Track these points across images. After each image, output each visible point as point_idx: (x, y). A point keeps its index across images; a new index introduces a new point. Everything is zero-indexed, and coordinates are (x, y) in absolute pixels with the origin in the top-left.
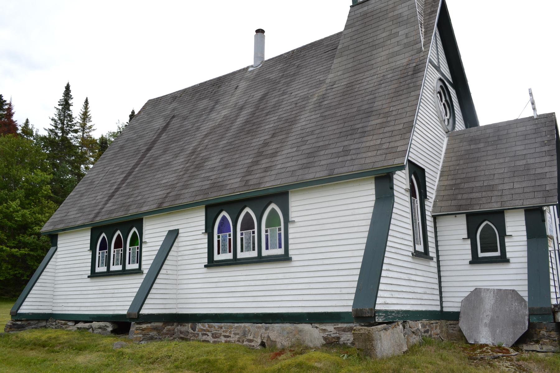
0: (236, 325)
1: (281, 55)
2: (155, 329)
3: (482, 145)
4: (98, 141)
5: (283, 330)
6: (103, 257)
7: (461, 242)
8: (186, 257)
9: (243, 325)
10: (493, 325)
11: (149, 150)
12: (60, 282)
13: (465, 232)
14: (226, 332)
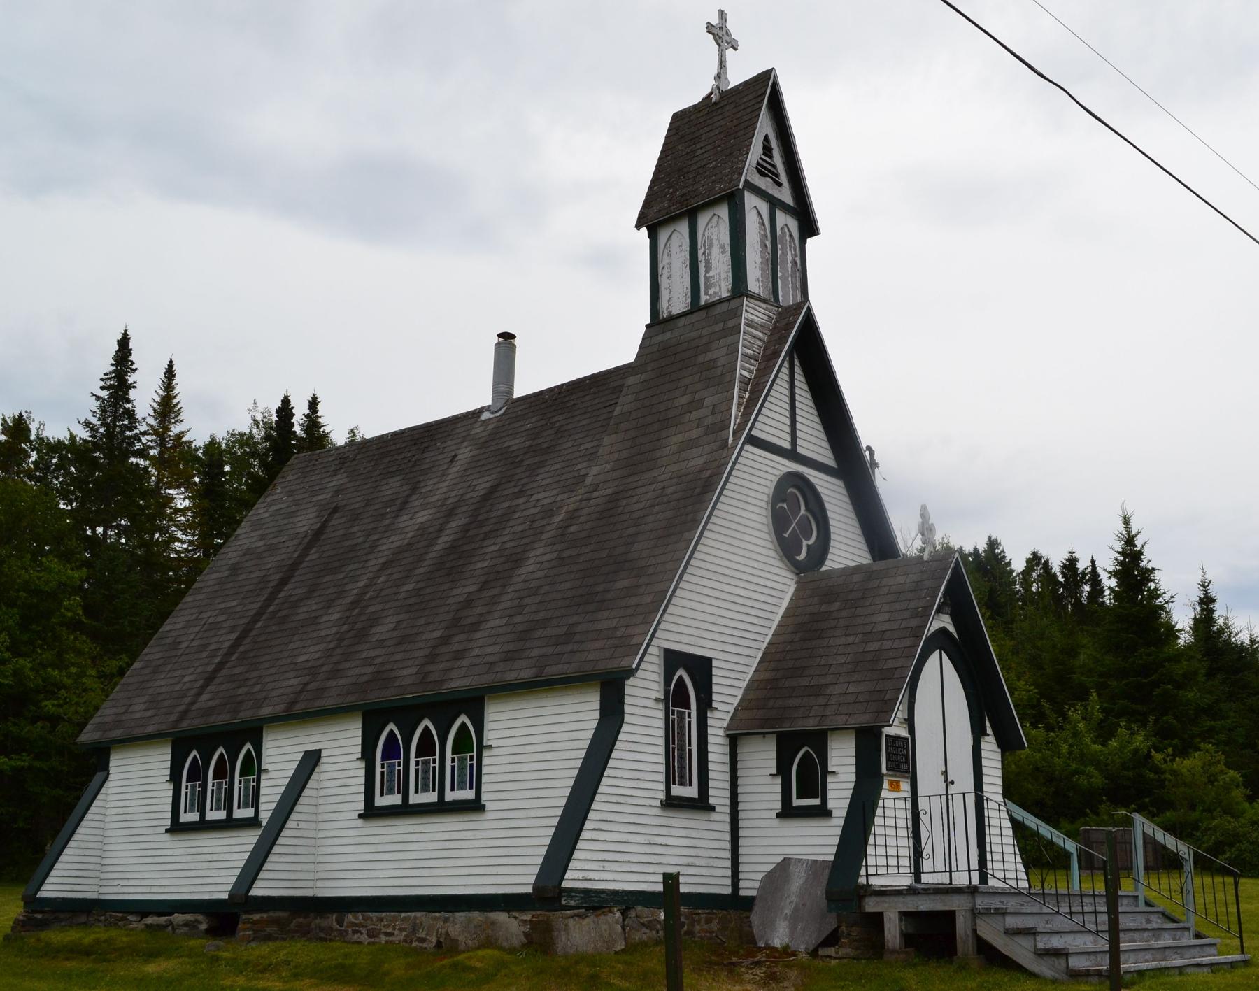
0: (403, 915)
1: (541, 393)
2: (276, 922)
3: (837, 605)
4: (200, 453)
5: (469, 921)
6: (193, 794)
7: (769, 780)
8: (332, 800)
9: (413, 914)
10: (794, 919)
11: (283, 582)
12: (113, 840)
13: (774, 763)
14: (387, 926)
